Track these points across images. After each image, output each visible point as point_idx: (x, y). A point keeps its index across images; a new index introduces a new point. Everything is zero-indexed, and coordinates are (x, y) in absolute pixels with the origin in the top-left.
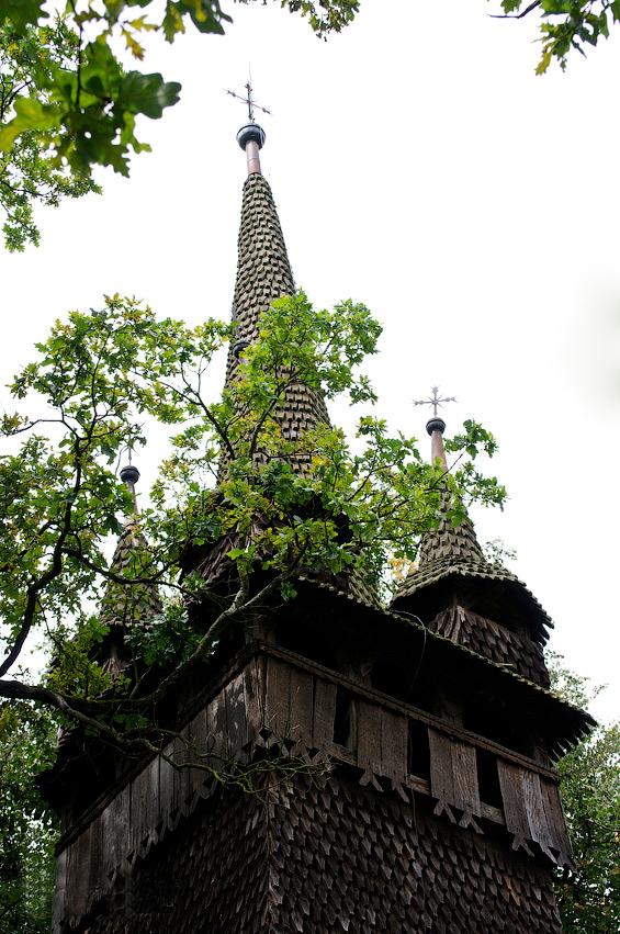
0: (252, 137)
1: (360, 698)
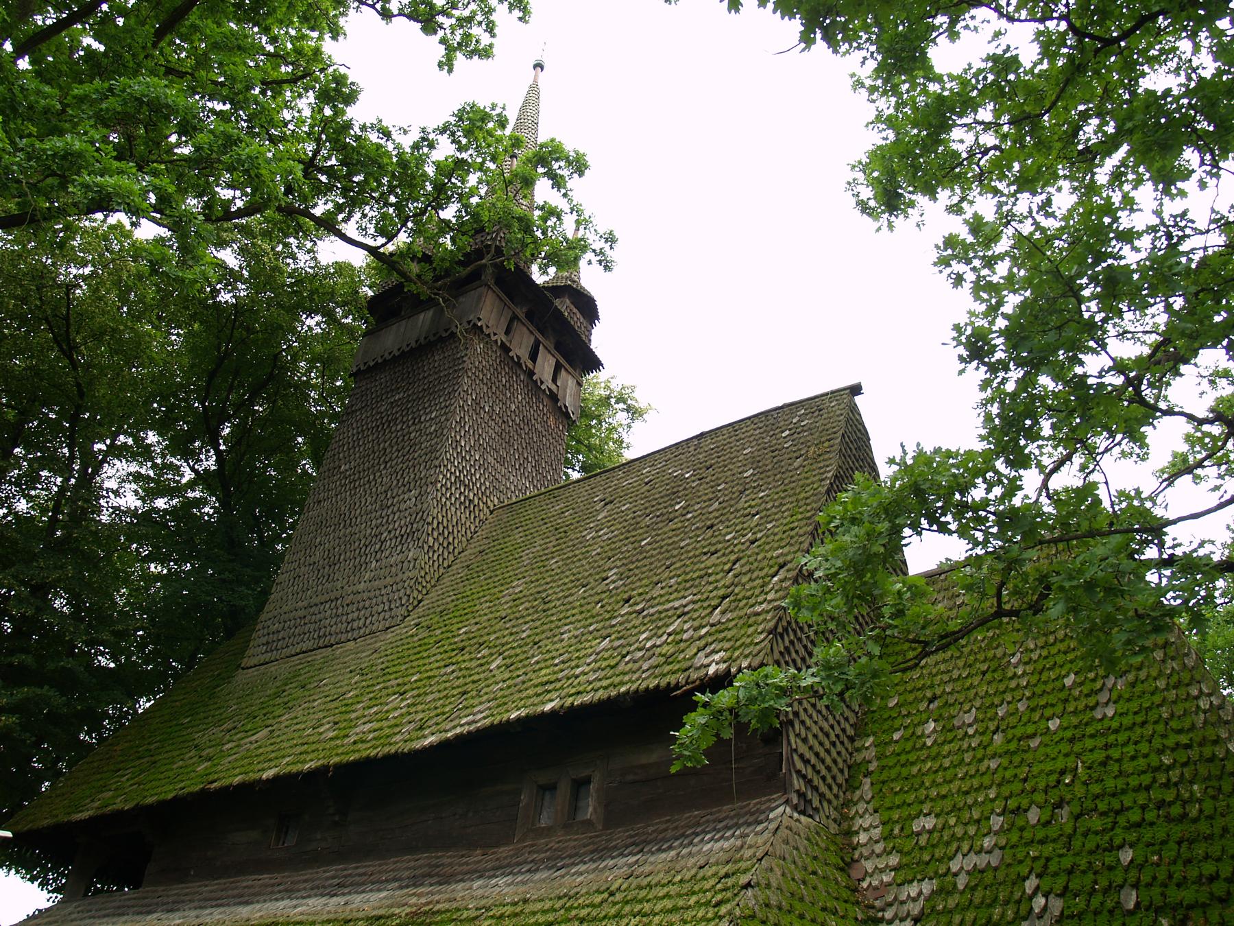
0: (539, 66)
1: (519, 319)
